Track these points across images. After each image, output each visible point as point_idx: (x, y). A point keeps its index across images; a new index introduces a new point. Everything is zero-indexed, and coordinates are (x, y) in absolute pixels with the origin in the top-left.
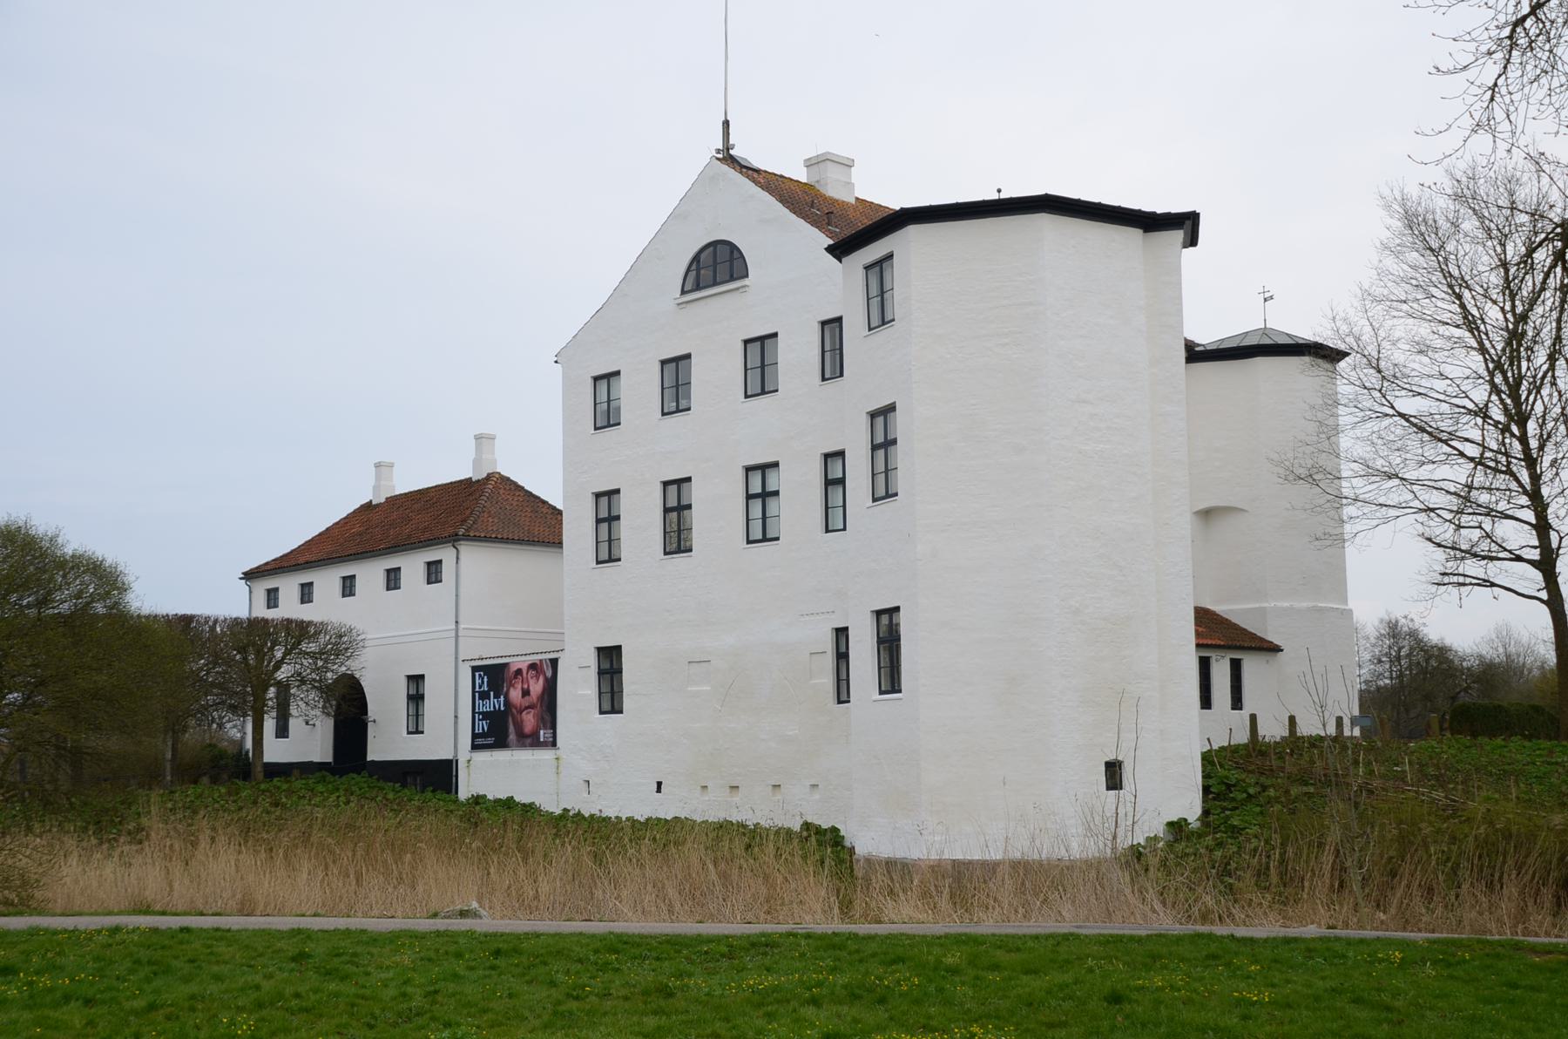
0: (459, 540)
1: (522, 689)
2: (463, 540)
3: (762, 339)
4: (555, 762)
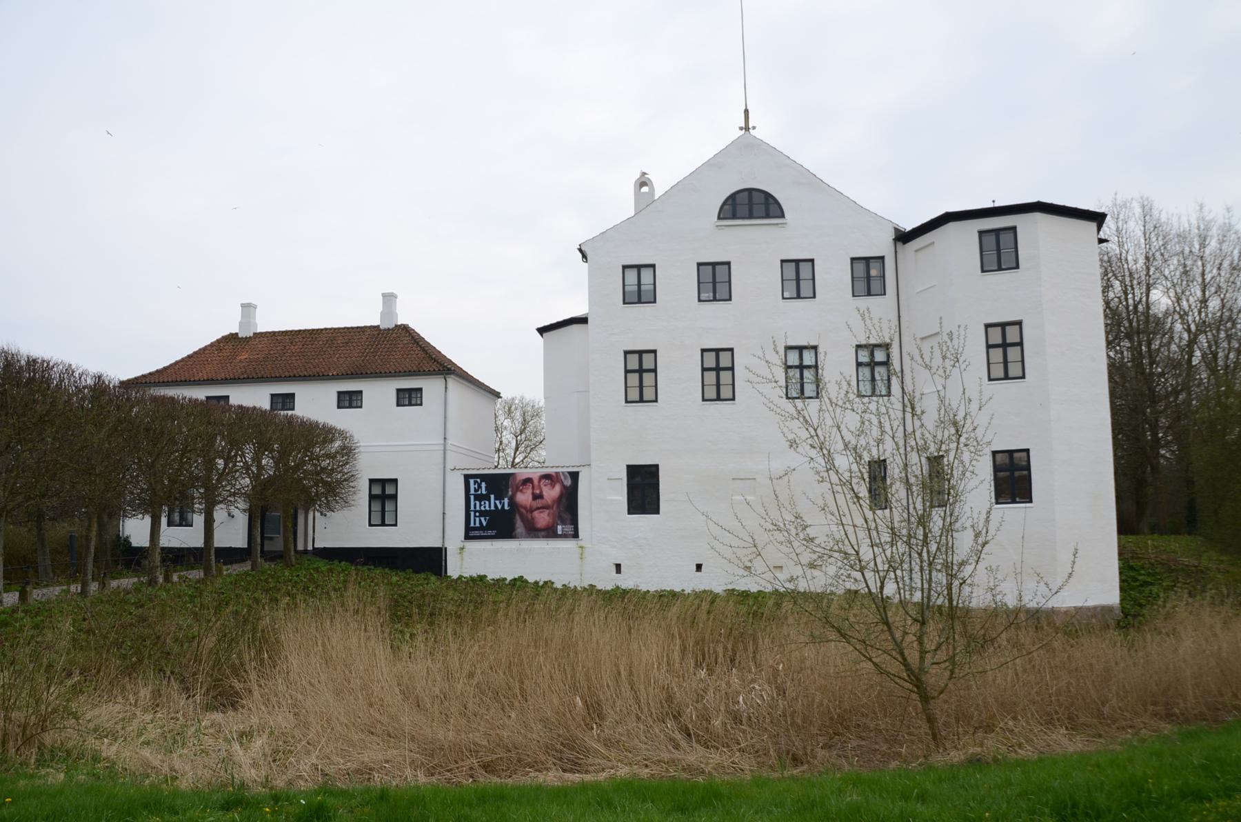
0: (450, 374)
1: (533, 494)
4: (579, 551)
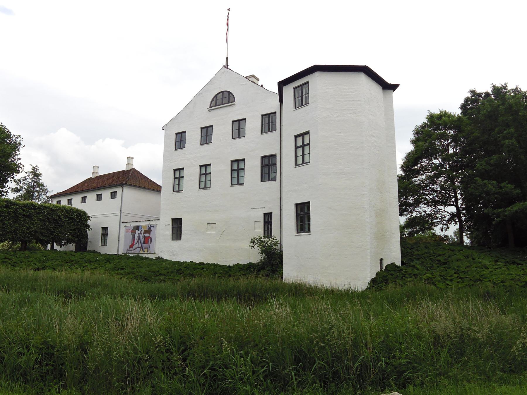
2: (125, 185)
3: (239, 121)
